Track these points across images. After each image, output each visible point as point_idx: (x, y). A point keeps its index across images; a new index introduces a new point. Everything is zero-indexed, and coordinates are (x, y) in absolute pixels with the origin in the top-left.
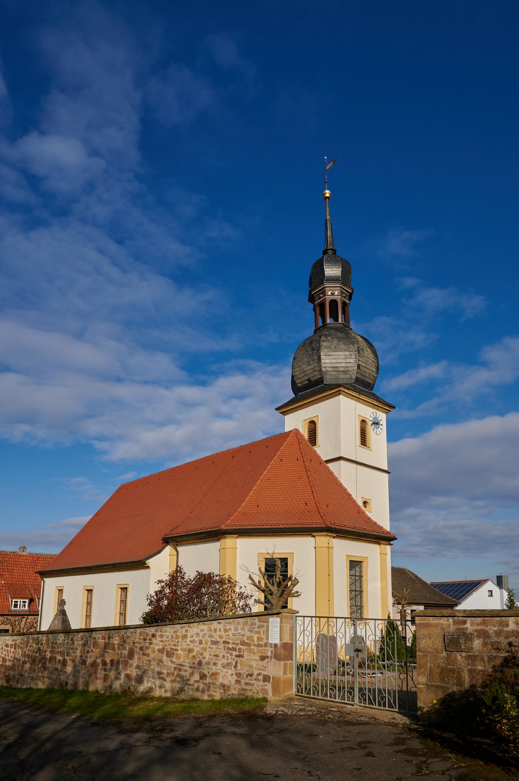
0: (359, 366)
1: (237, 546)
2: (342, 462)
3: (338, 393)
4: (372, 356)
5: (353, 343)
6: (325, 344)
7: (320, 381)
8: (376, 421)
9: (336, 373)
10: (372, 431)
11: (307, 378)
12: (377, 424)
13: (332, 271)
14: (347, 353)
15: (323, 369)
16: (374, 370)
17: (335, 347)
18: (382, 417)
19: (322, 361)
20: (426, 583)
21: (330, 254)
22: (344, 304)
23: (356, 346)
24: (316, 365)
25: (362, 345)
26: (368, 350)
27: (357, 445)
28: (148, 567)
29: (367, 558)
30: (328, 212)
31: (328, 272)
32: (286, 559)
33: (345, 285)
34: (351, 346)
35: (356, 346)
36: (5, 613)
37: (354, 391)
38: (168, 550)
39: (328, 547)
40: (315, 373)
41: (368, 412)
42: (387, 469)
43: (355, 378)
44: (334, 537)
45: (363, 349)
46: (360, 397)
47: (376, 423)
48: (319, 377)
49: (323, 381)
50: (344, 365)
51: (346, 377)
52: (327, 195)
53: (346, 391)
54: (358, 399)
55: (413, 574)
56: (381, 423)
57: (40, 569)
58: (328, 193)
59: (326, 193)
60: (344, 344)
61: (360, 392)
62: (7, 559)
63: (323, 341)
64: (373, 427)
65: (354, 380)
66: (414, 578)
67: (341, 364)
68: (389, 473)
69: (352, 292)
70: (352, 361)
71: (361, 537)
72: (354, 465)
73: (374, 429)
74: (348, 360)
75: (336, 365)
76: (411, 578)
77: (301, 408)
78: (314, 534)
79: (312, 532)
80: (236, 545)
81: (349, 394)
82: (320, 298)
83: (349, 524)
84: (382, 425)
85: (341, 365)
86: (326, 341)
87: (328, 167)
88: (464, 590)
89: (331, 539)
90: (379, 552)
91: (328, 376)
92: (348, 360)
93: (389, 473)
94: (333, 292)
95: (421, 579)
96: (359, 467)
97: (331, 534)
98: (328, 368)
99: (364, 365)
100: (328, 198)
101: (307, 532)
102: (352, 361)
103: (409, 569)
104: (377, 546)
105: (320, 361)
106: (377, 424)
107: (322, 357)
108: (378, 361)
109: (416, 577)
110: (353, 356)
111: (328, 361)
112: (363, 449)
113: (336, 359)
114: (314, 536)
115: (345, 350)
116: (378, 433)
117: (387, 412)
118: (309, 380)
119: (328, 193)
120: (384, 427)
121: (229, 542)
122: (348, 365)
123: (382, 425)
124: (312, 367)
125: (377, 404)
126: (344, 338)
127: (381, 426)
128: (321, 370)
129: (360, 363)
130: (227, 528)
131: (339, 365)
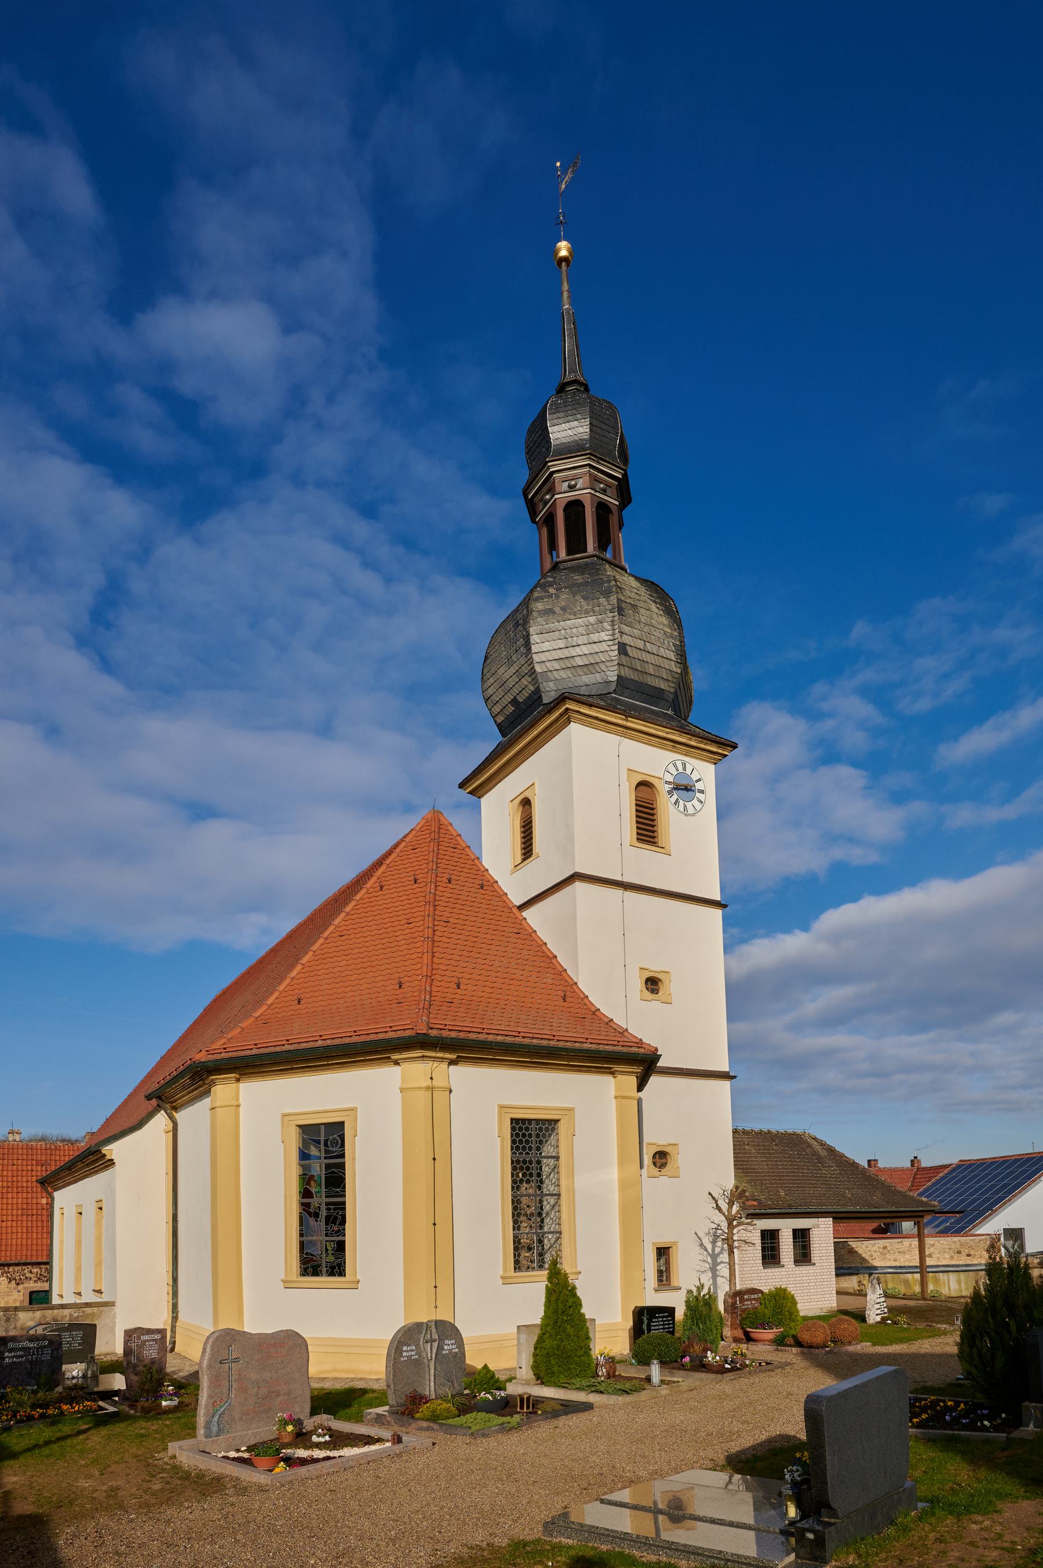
0: (623, 649)
1: (241, 1101)
2: (578, 886)
3: (566, 719)
4: (664, 620)
5: (607, 594)
6: (540, 606)
7: (536, 697)
8: (684, 782)
9: (568, 672)
10: (671, 807)
11: (509, 698)
12: (688, 789)
13: (564, 430)
14: (592, 619)
15: (538, 668)
16: (672, 655)
17: (563, 609)
18: (704, 772)
19: (534, 648)
20: (854, 1165)
21: (571, 392)
22: (602, 509)
23: (613, 599)
24: (522, 660)
25: (633, 595)
26: (653, 606)
27: (626, 842)
28: (111, 1163)
29: (571, 1110)
30: (565, 295)
31: (558, 435)
32: (338, 1128)
33: (599, 459)
34: (602, 600)
35: (613, 599)
36: (39, 1260)
37: (611, 708)
38: (160, 1121)
39: (431, 1089)
40: (523, 680)
41: (659, 762)
42: (718, 898)
43: (615, 678)
44: (452, 1062)
45: (634, 606)
46: (629, 724)
47: (684, 788)
48: (532, 688)
49: (540, 697)
50: (585, 650)
51: (594, 681)
52: (564, 253)
53: (585, 710)
54: (625, 731)
55: (822, 1144)
56: (699, 786)
57: (41, 1172)
58: (563, 249)
59: (559, 250)
60: (585, 598)
61: (628, 712)
62: (58, 1158)
63: (537, 599)
64: (675, 797)
65: (613, 686)
66: (823, 1153)
67: (577, 649)
68: (725, 906)
69: (625, 475)
70: (603, 636)
71: (542, 1057)
72: (617, 893)
73: (676, 802)
74: (595, 637)
75: (566, 653)
76: (815, 1153)
77: (505, 772)
78: (395, 1056)
79: (388, 1051)
80: (237, 1098)
81: (596, 718)
82: (546, 502)
83: (564, 1032)
84: (702, 792)
85: (578, 651)
86: (542, 598)
87: (563, 186)
88: (1024, 1172)
89: (445, 1065)
90: (613, 1093)
91: (551, 684)
92: (595, 637)
93: (725, 906)
94: (574, 482)
95: (843, 1155)
96: (630, 896)
97: (433, 1054)
98: (548, 664)
99: (640, 644)
100: (564, 259)
101: (376, 1052)
102: (603, 636)
103: (813, 1133)
104: (609, 1079)
105: (529, 649)
106: (688, 789)
107: (534, 638)
108: (681, 633)
109: (831, 1150)
110: (605, 625)
111: (546, 646)
112: (646, 854)
113: (572, 642)
114: (612, 1073)
115: (587, 612)
116: (691, 810)
117: (717, 759)
118: (514, 702)
119: (563, 249)
120: (710, 798)
121: (223, 1090)
122: (595, 648)
123: (702, 792)
124: (516, 667)
125: (715, 750)
126: (586, 584)
127: (698, 795)
128: (532, 672)
129: (626, 639)
130: (211, 1057)
131: (573, 652)
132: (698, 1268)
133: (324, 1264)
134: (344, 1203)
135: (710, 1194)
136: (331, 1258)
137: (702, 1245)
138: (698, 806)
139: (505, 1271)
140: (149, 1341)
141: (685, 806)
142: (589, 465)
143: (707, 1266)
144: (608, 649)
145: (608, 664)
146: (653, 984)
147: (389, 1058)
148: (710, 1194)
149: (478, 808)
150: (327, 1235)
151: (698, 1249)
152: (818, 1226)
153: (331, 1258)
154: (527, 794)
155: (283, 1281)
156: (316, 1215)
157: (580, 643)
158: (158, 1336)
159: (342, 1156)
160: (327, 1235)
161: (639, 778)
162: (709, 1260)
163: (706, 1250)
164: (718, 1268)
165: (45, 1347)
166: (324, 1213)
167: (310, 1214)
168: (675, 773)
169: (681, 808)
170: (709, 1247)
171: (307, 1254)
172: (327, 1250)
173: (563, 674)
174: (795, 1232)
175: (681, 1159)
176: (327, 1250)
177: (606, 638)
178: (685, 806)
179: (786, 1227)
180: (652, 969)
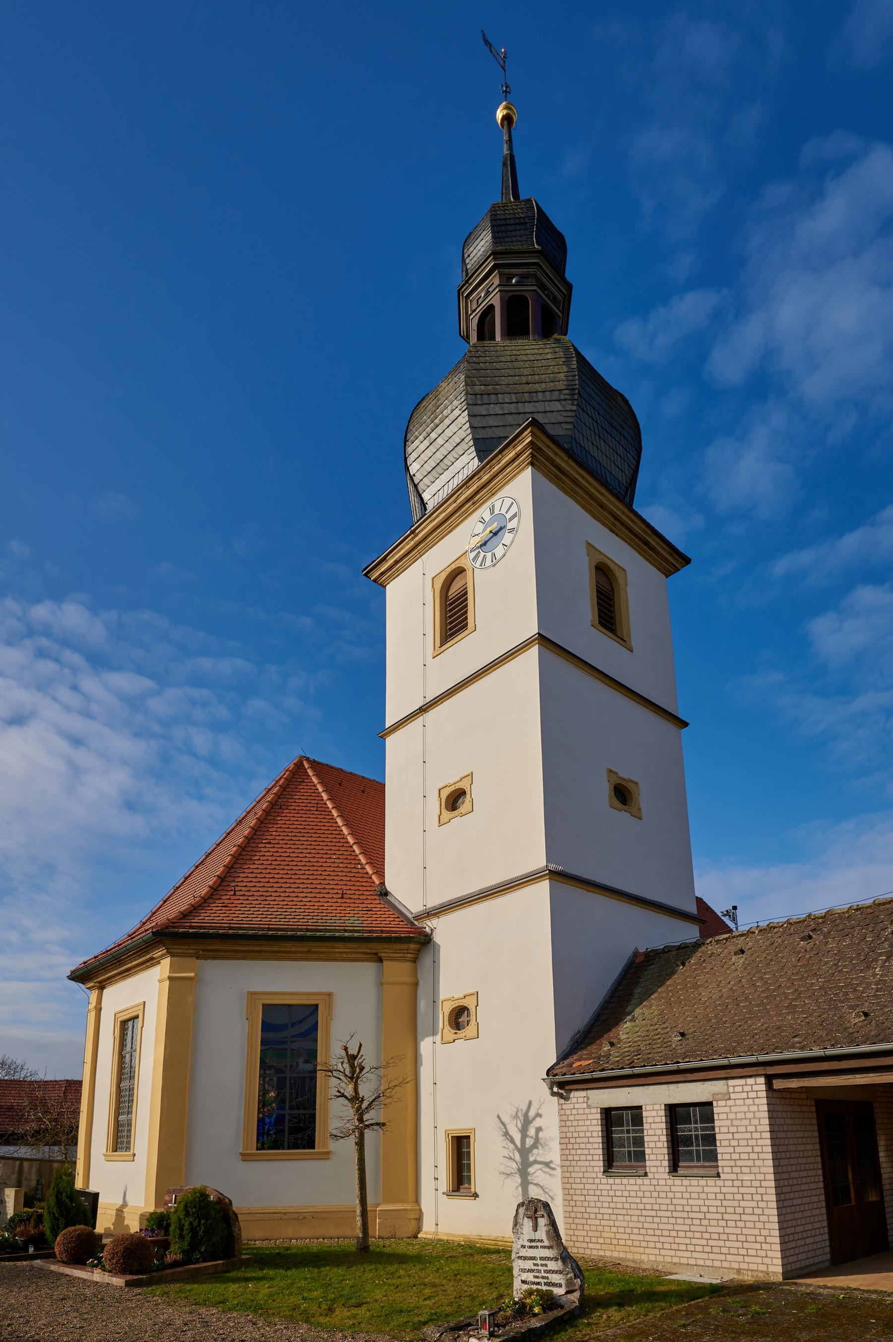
116: (514, 509)
132: (502, 1169)
135: (498, 1117)
137: (506, 1134)
142: (537, 264)
143: (514, 1166)
146: (455, 800)
148: (498, 1117)
151: (500, 1141)
152: (727, 1097)
155: (242, 1154)
157: (558, 403)
162: (517, 1157)
163: (512, 1141)
164: (531, 1170)
169: (514, 509)
170: (517, 1137)
174: (676, 1114)
175: (484, 1015)
179: (653, 1101)
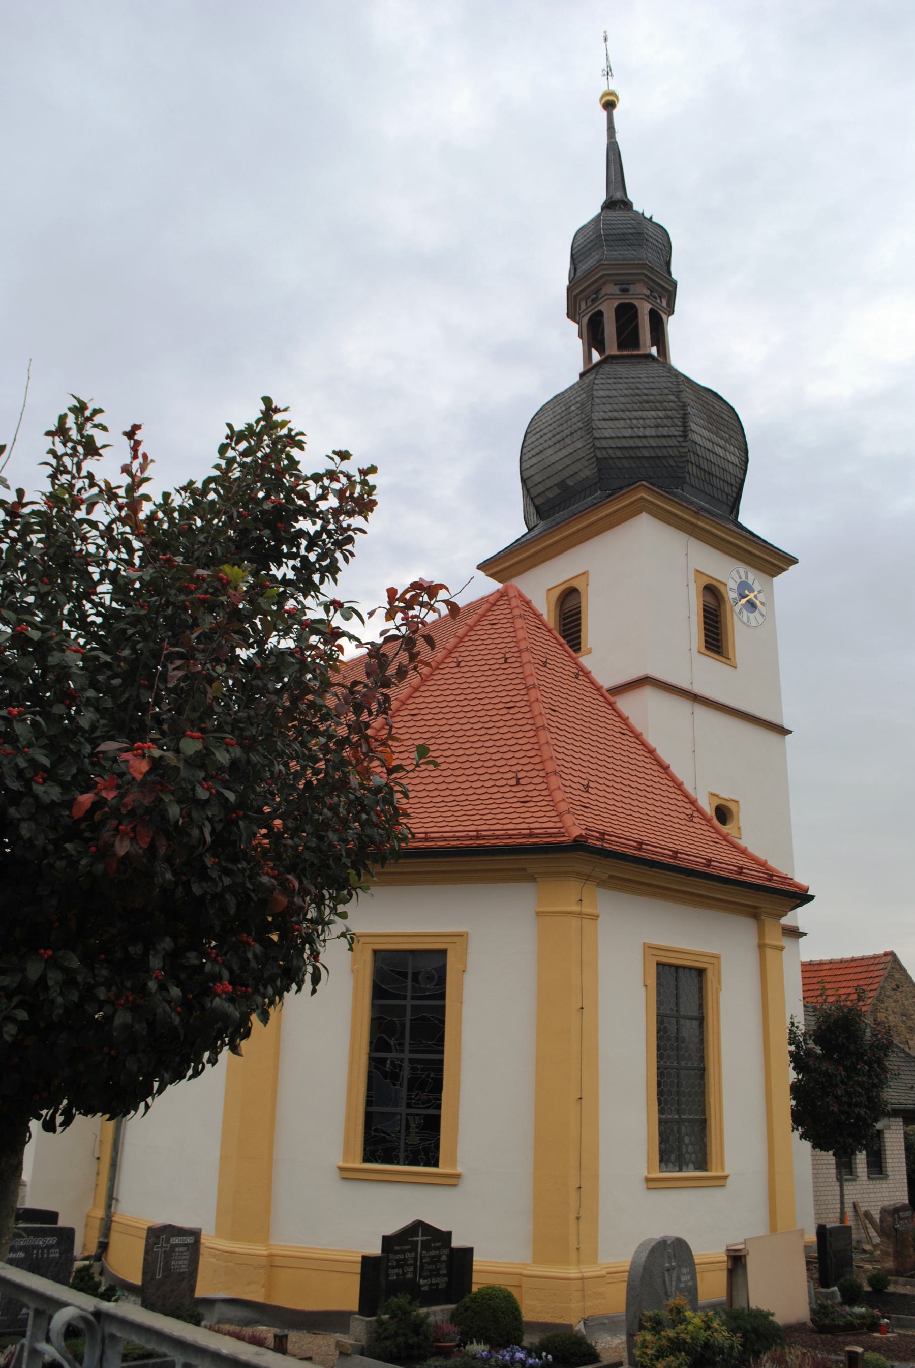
2: (648, 694)
116: (754, 623)
133: (402, 1147)
134: (441, 1062)
136: (415, 1139)
138: (760, 619)
139: (649, 1170)
140: (180, 1246)
141: (748, 618)
144: (677, 444)
145: (676, 459)
147: (524, 870)
149: (771, 585)
150: (409, 1106)
153: (415, 1139)
154: (575, 584)
156: (395, 1076)
158: (190, 1240)
159: (442, 996)
160: (409, 1106)
161: (706, 581)
165: (51, 1247)
166: (406, 1073)
167: (385, 1075)
168: (739, 581)
171: (376, 1130)
172: (408, 1127)
173: (626, 463)
176: (408, 1127)
177: (676, 434)
178: (748, 618)
180: (722, 795)
